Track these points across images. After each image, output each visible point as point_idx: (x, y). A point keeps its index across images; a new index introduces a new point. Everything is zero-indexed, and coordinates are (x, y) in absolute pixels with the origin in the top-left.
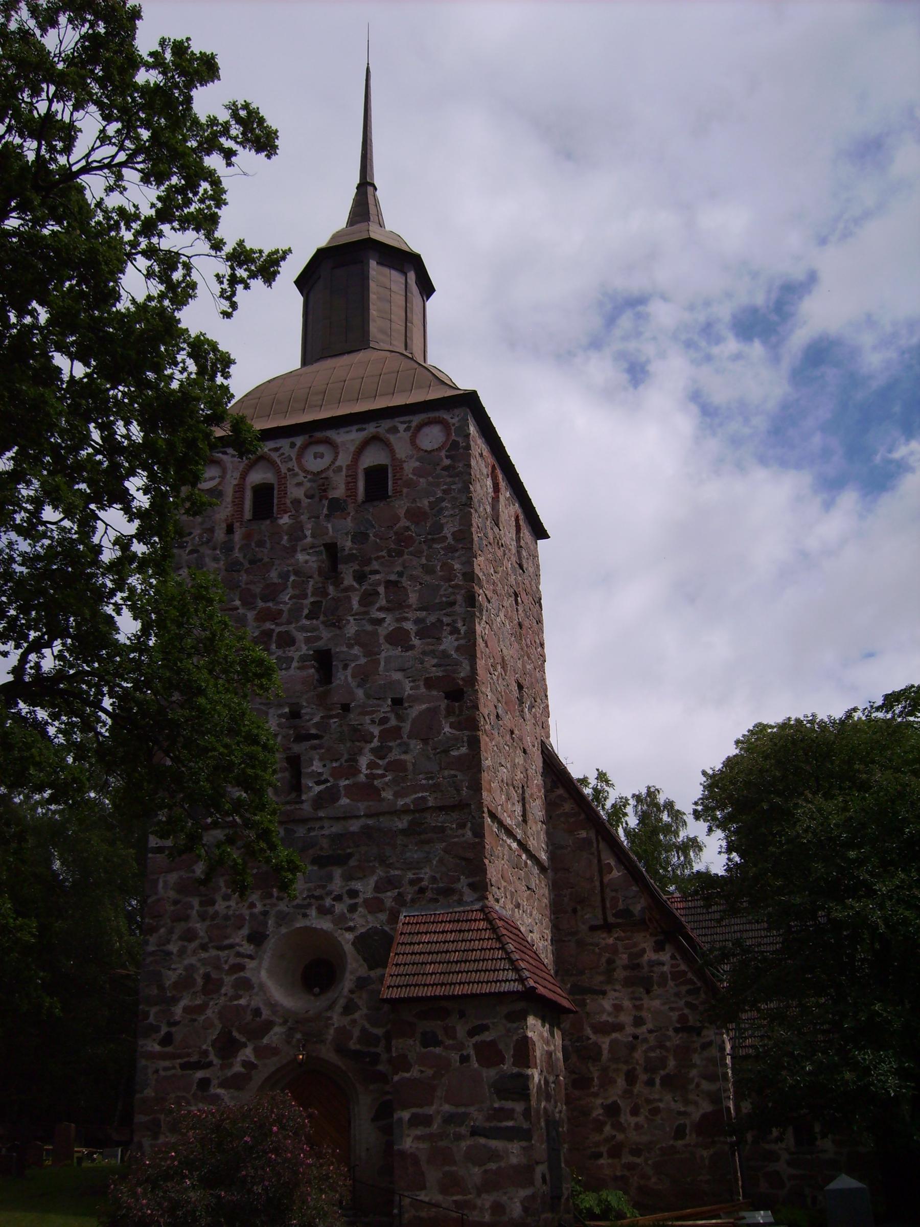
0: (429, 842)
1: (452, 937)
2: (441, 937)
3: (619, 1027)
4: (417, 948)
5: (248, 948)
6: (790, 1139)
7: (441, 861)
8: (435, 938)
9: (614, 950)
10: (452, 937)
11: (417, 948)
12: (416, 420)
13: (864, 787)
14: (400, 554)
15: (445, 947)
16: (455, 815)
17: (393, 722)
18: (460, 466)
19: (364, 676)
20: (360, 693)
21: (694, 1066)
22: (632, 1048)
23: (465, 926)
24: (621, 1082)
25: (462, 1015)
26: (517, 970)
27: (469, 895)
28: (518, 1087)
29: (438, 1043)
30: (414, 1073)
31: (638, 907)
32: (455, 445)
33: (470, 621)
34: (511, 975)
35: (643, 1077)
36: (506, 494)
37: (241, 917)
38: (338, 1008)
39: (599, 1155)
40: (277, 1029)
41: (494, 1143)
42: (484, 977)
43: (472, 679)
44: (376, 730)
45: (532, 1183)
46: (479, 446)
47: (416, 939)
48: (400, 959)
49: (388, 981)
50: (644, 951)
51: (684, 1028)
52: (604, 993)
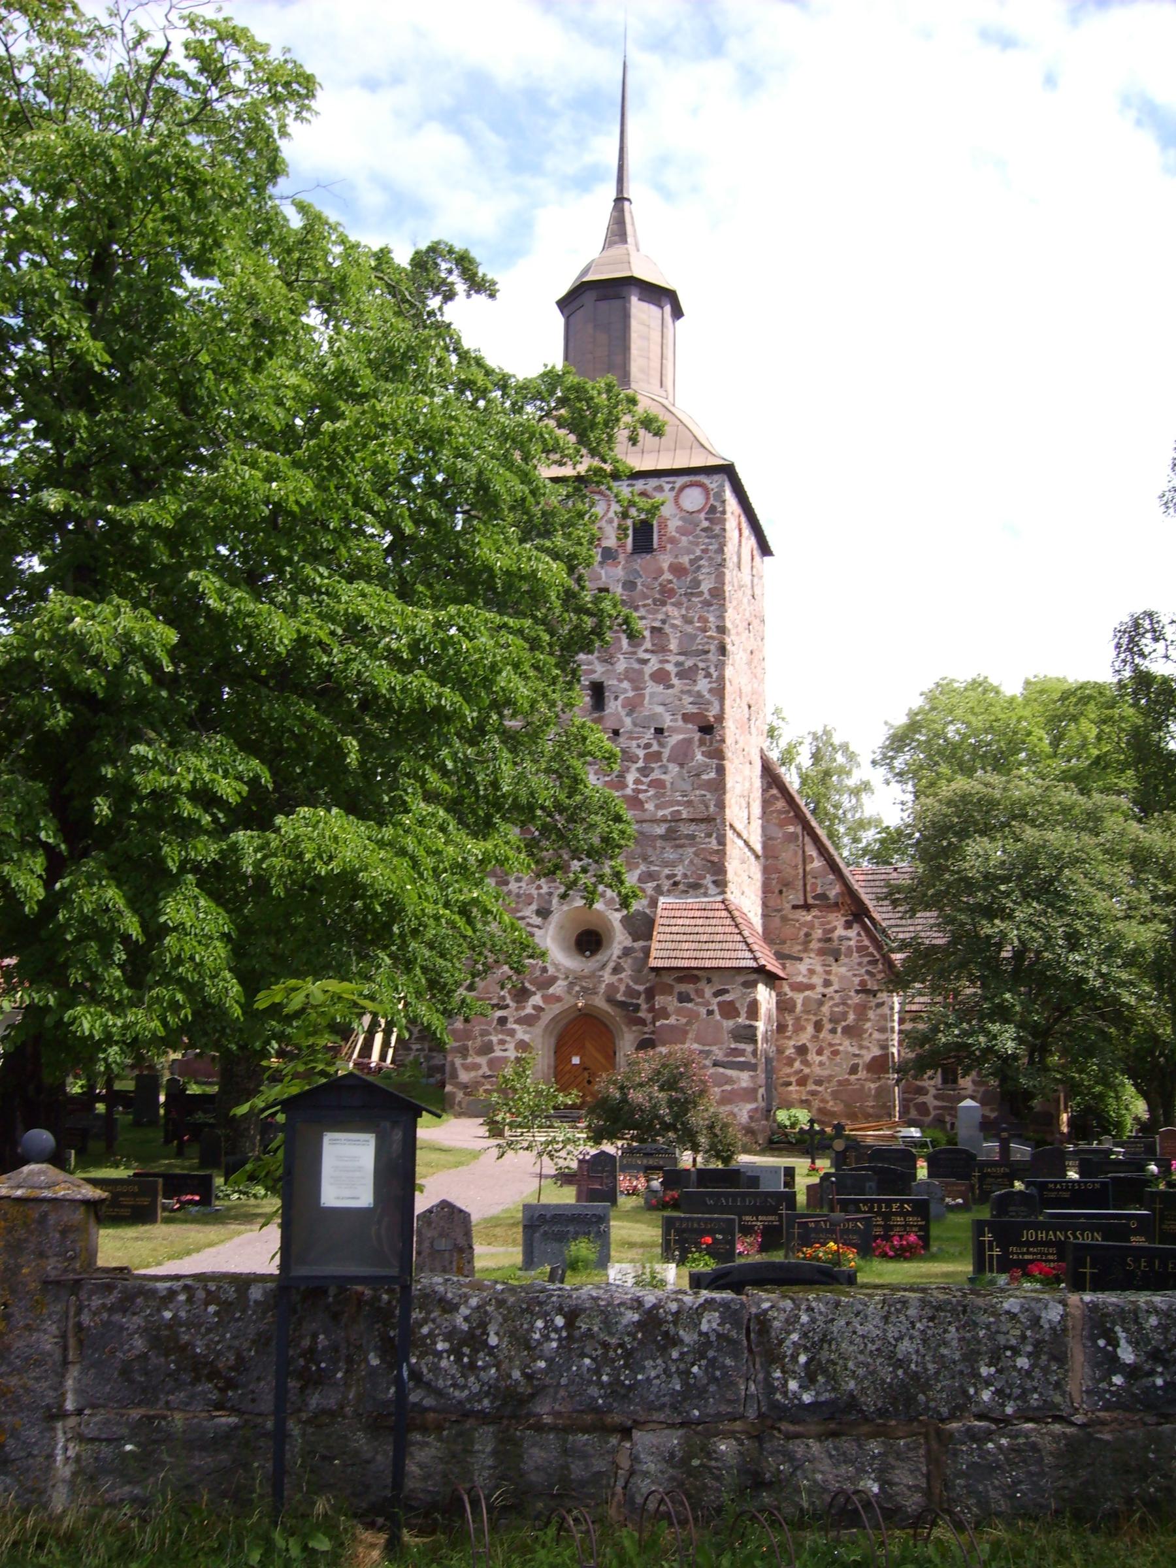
0: (682, 846)
1: (700, 922)
2: (693, 922)
3: (811, 987)
4: (674, 929)
5: (537, 920)
6: (938, 1079)
7: (691, 862)
8: (687, 922)
9: (811, 926)
10: (700, 922)
11: (674, 929)
12: (680, 481)
13: (1018, 839)
14: (664, 604)
15: (696, 930)
16: (703, 826)
17: (655, 747)
18: (717, 529)
19: (632, 707)
20: (628, 721)
21: (869, 1020)
22: (821, 1003)
23: (710, 914)
24: (810, 1029)
25: (709, 981)
26: (751, 950)
27: (713, 890)
28: (749, 1035)
29: (690, 1000)
30: (672, 1021)
31: (834, 891)
32: (713, 509)
33: (721, 666)
34: (748, 955)
35: (828, 1026)
36: (747, 531)
37: (530, 896)
38: (609, 969)
39: (789, 1084)
40: (560, 982)
41: (729, 1072)
42: (727, 954)
43: (720, 718)
44: (641, 753)
45: (756, 1100)
46: (732, 504)
47: (673, 921)
48: (662, 937)
49: (653, 953)
50: (835, 928)
51: (863, 990)
52: (801, 959)
